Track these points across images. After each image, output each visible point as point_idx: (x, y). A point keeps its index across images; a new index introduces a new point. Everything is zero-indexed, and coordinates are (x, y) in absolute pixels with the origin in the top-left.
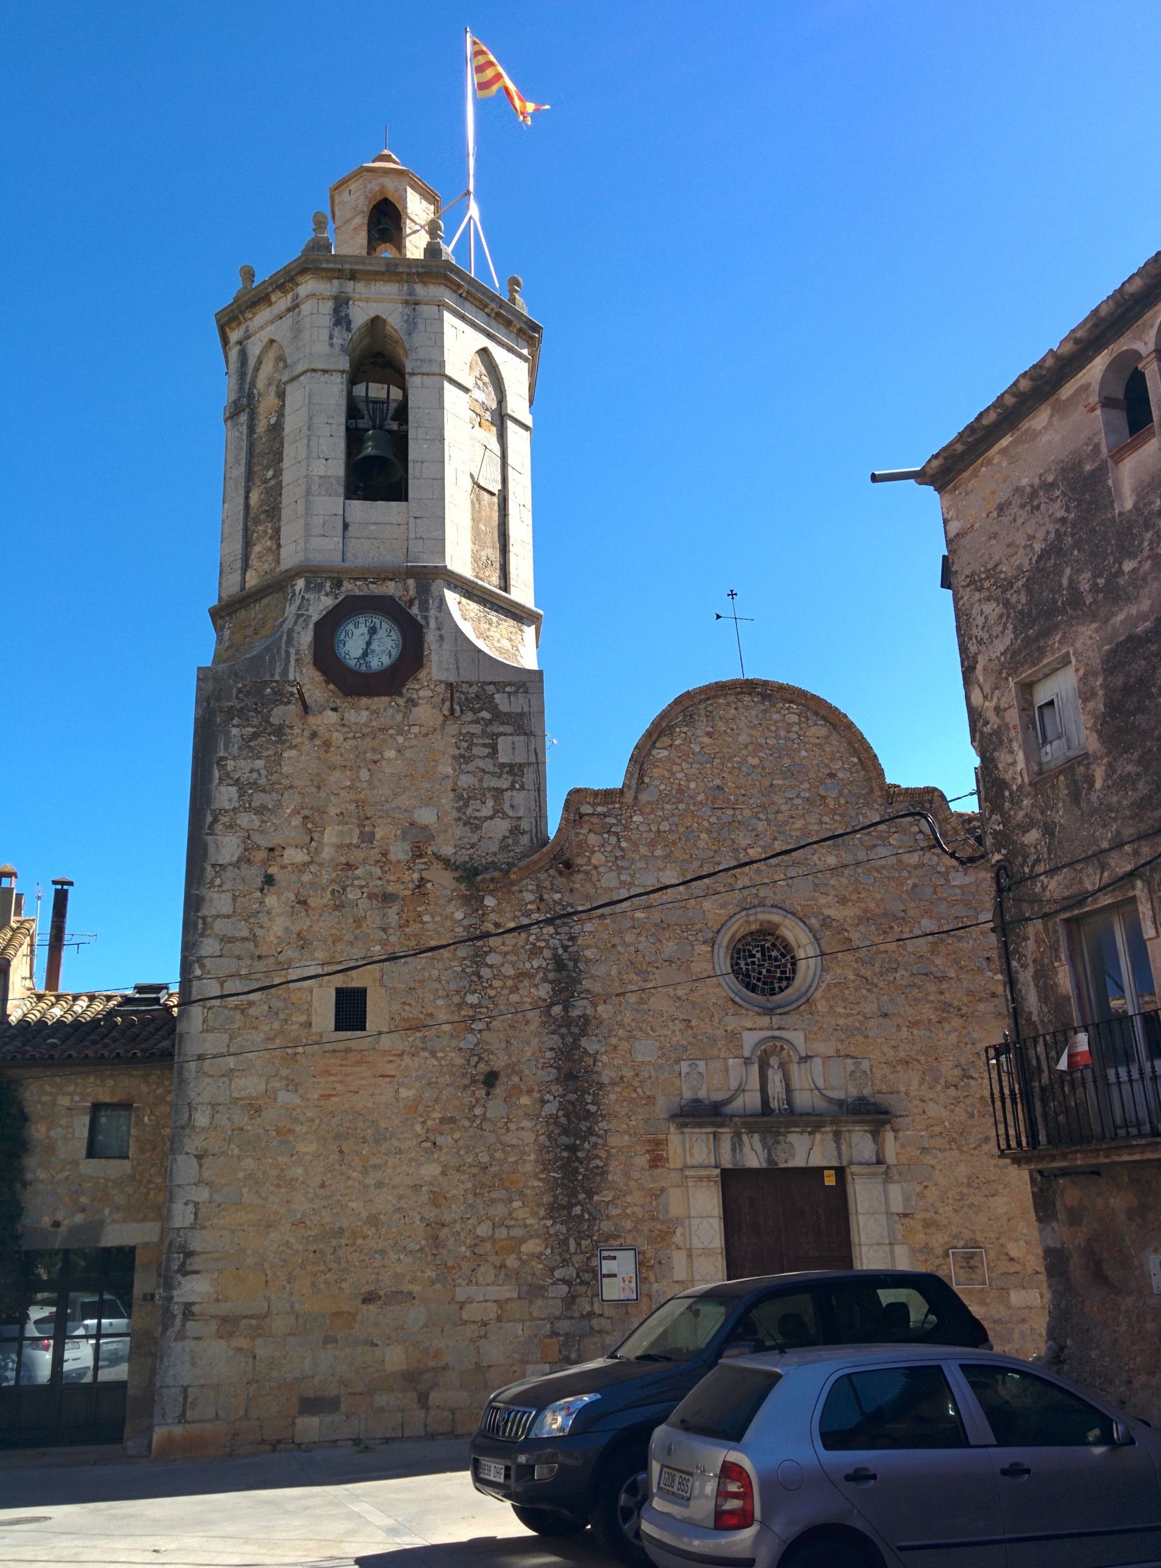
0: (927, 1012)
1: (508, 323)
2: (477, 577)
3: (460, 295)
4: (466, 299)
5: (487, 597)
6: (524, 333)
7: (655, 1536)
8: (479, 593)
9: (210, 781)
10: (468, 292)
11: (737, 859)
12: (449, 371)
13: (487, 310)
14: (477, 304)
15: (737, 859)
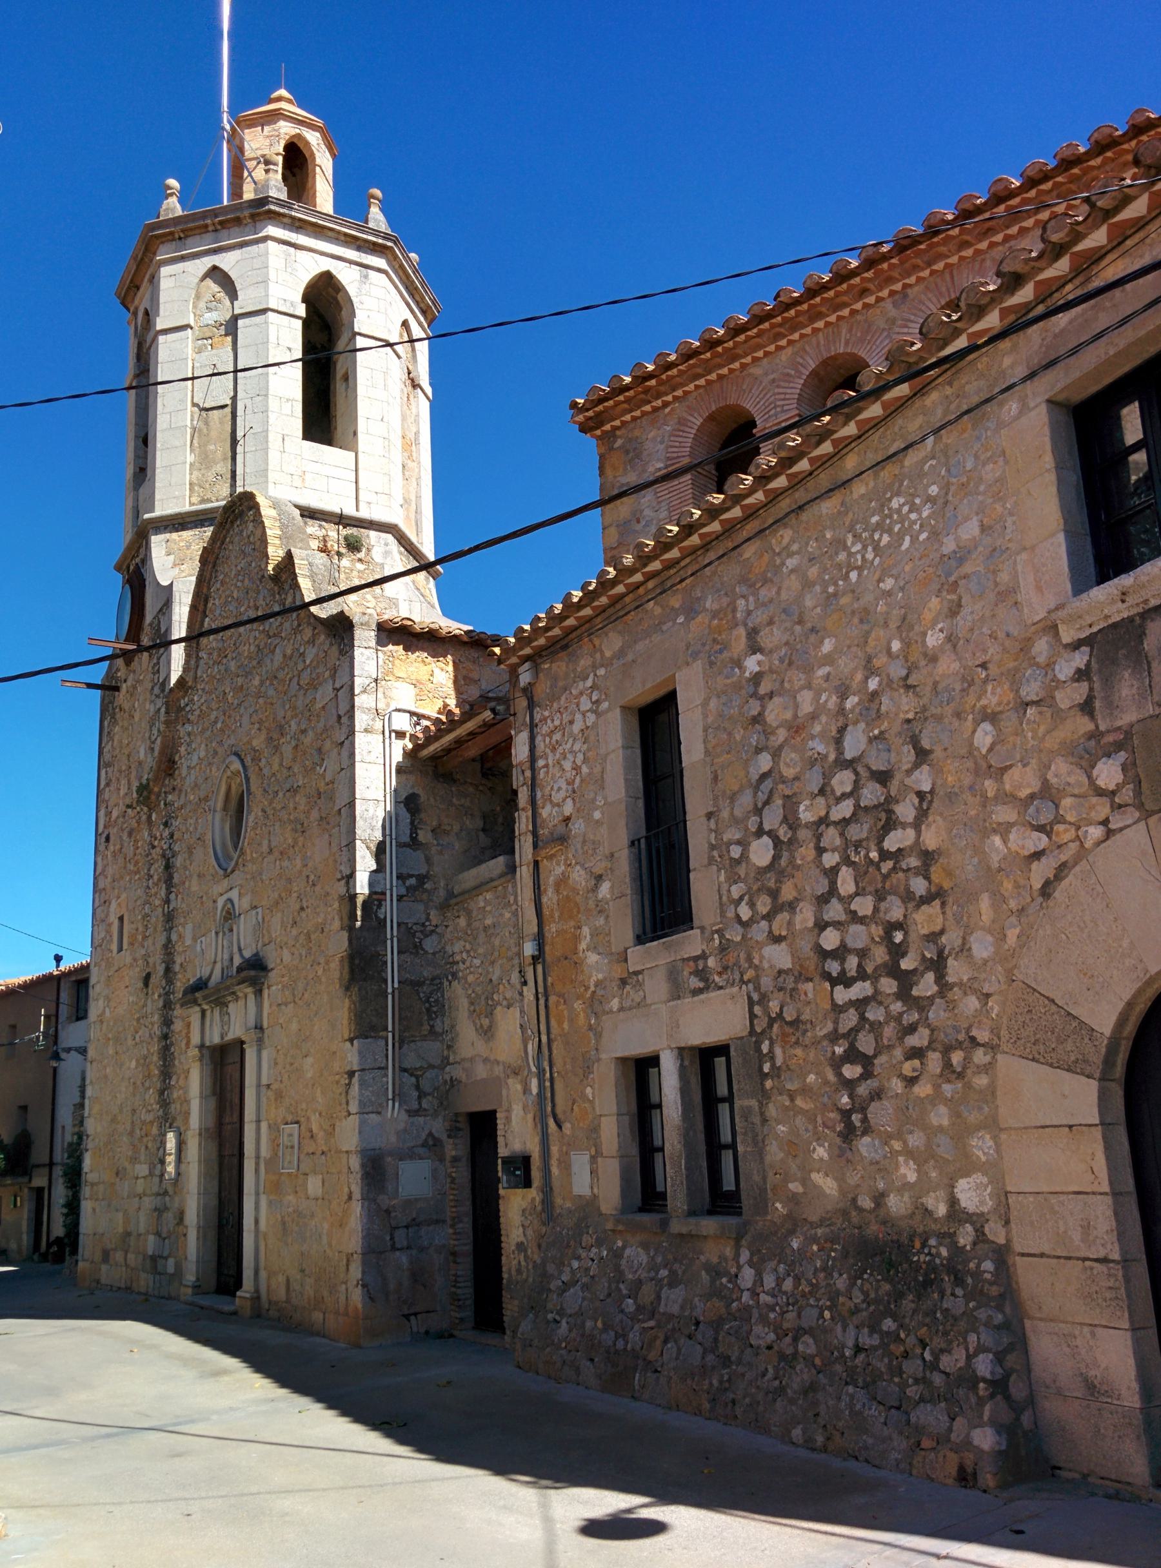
0: (710, 719)
1: (238, 221)
2: (203, 501)
3: (180, 238)
4: (186, 237)
5: (201, 517)
6: (259, 214)
7: (1138, 422)
8: (193, 519)
9: (687, 1157)
10: (183, 231)
11: (1093, 1334)
12: (428, 403)
13: (210, 228)
14: (198, 231)
15: (1093, 1334)
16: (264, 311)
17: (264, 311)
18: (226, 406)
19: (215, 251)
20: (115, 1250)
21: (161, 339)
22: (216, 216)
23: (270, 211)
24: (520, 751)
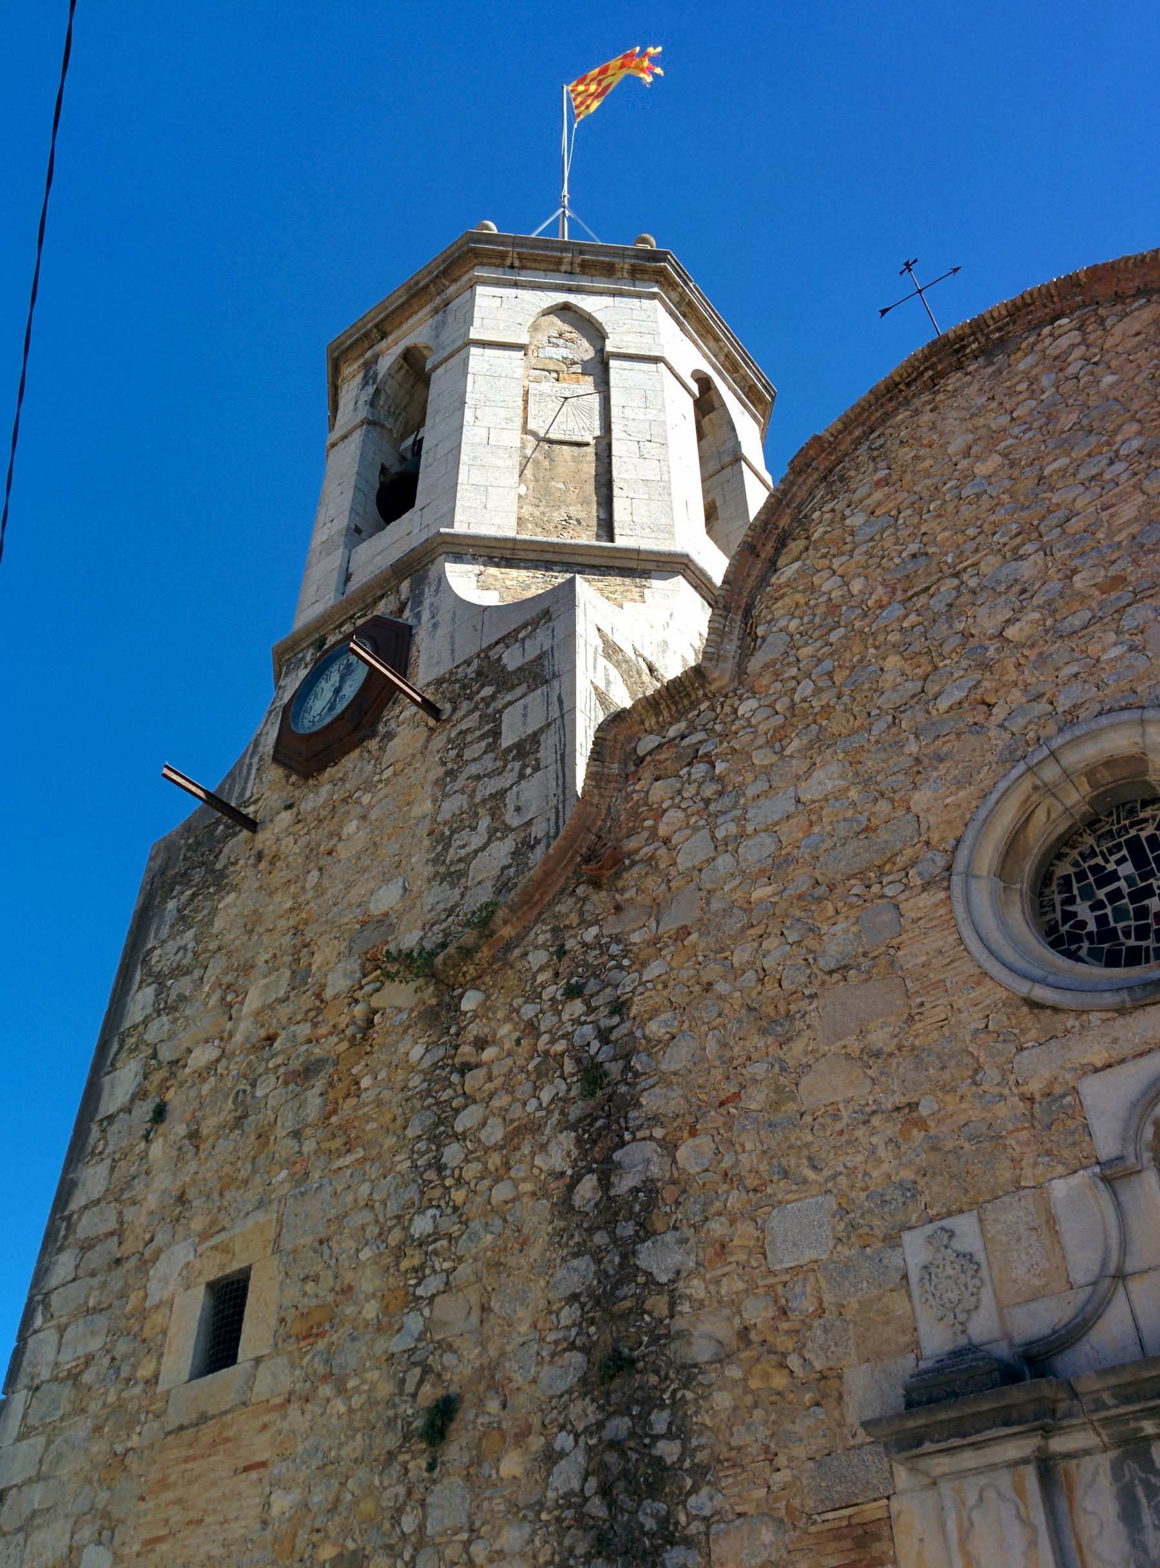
6: (644, 271)
14: (544, 266)
16: (656, 360)
17: (656, 360)
18: (587, 444)
19: (570, 290)
20: (1143, 735)
21: (474, 351)
22: (581, 253)
23: (662, 272)
24: (1075, 1421)
